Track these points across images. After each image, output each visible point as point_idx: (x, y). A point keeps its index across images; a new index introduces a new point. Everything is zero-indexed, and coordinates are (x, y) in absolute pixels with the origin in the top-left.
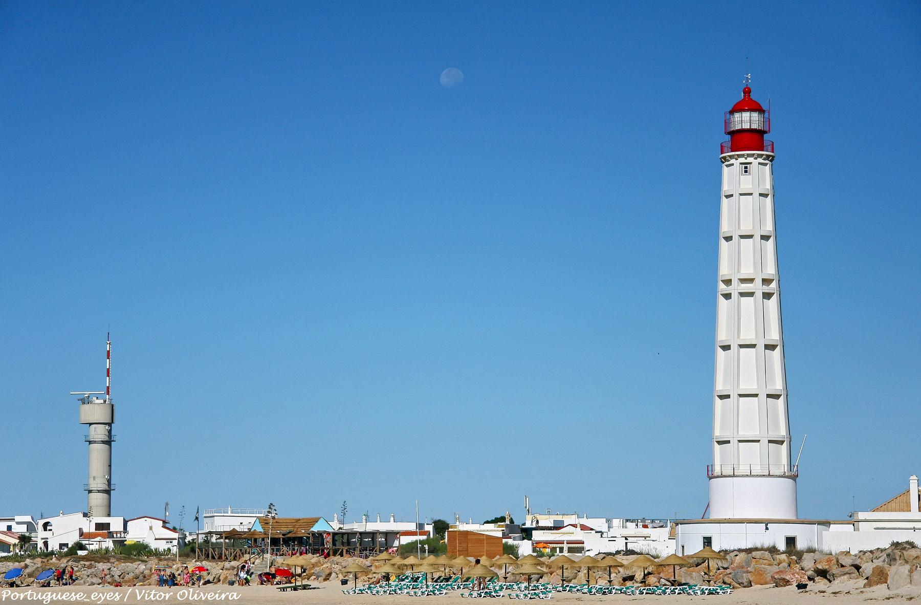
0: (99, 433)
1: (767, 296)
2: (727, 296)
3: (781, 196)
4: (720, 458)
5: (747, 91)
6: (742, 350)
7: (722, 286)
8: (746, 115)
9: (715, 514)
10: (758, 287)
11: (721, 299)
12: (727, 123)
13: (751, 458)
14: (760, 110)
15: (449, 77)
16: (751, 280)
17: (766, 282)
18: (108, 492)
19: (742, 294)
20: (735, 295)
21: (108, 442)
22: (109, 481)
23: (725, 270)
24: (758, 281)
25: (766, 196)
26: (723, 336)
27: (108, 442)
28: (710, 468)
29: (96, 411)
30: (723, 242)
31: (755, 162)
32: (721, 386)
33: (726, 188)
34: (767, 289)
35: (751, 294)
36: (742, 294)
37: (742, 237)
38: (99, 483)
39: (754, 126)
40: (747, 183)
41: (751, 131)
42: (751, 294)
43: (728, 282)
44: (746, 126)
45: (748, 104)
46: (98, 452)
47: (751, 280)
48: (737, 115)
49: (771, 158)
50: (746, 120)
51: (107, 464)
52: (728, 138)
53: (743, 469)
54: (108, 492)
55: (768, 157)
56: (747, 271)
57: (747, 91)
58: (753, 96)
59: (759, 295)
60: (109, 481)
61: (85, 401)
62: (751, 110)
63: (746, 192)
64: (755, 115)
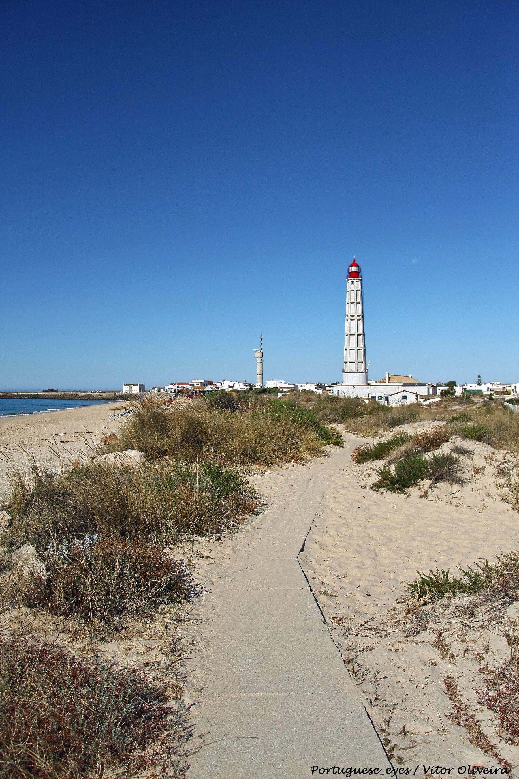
0: (259, 360)
1: (358, 320)
2: (347, 320)
5: (354, 261)
7: (346, 317)
8: (353, 267)
10: (355, 318)
12: (349, 270)
14: (357, 265)
15: (414, 261)
16: (354, 316)
17: (358, 316)
18: (262, 375)
19: (351, 320)
21: (262, 362)
22: (262, 372)
23: (347, 313)
27: (262, 362)
28: (343, 370)
29: (258, 354)
32: (346, 347)
34: (358, 318)
35: (354, 320)
36: (351, 320)
38: (260, 373)
40: (353, 287)
41: (354, 272)
42: (354, 320)
44: (353, 271)
45: (354, 264)
46: (259, 365)
47: (354, 316)
50: (354, 269)
51: (108, 390)
52: (349, 274)
53: (350, 371)
54: (262, 375)
56: (353, 312)
57: (354, 261)
58: (356, 262)
60: (262, 372)
64: (356, 267)
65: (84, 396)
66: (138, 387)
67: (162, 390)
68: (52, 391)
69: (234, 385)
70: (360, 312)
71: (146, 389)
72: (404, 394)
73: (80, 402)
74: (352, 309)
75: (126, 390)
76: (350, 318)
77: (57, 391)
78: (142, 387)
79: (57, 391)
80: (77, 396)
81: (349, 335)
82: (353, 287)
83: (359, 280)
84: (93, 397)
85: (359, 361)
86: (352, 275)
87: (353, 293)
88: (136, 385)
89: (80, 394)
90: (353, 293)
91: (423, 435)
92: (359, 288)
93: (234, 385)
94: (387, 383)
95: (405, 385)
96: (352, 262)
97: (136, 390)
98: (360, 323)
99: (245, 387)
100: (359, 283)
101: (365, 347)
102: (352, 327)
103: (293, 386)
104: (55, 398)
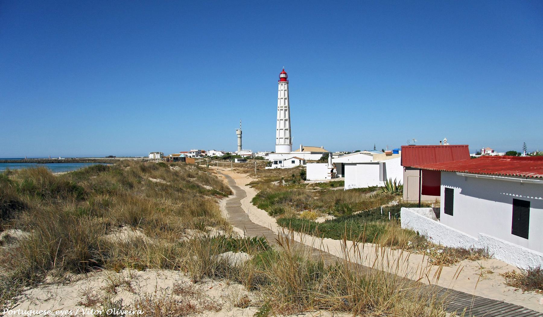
0: (239, 136)
1: (286, 110)
10: (284, 108)
14: (285, 73)
21: (241, 138)
23: (279, 105)
29: (238, 132)
38: (239, 144)
40: (282, 88)
42: (282, 110)
46: (239, 140)
49: (288, 83)
50: (283, 76)
68: (111, 157)
70: (287, 104)
72: (293, 159)
74: (281, 103)
79: (115, 157)
82: (282, 87)
85: (286, 137)
86: (285, 79)
88: (158, 153)
91: (220, 211)
92: (286, 88)
94: (301, 152)
95: (312, 153)
98: (287, 112)
100: (286, 86)
101: (290, 128)
102: (281, 115)
103: (251, 153)
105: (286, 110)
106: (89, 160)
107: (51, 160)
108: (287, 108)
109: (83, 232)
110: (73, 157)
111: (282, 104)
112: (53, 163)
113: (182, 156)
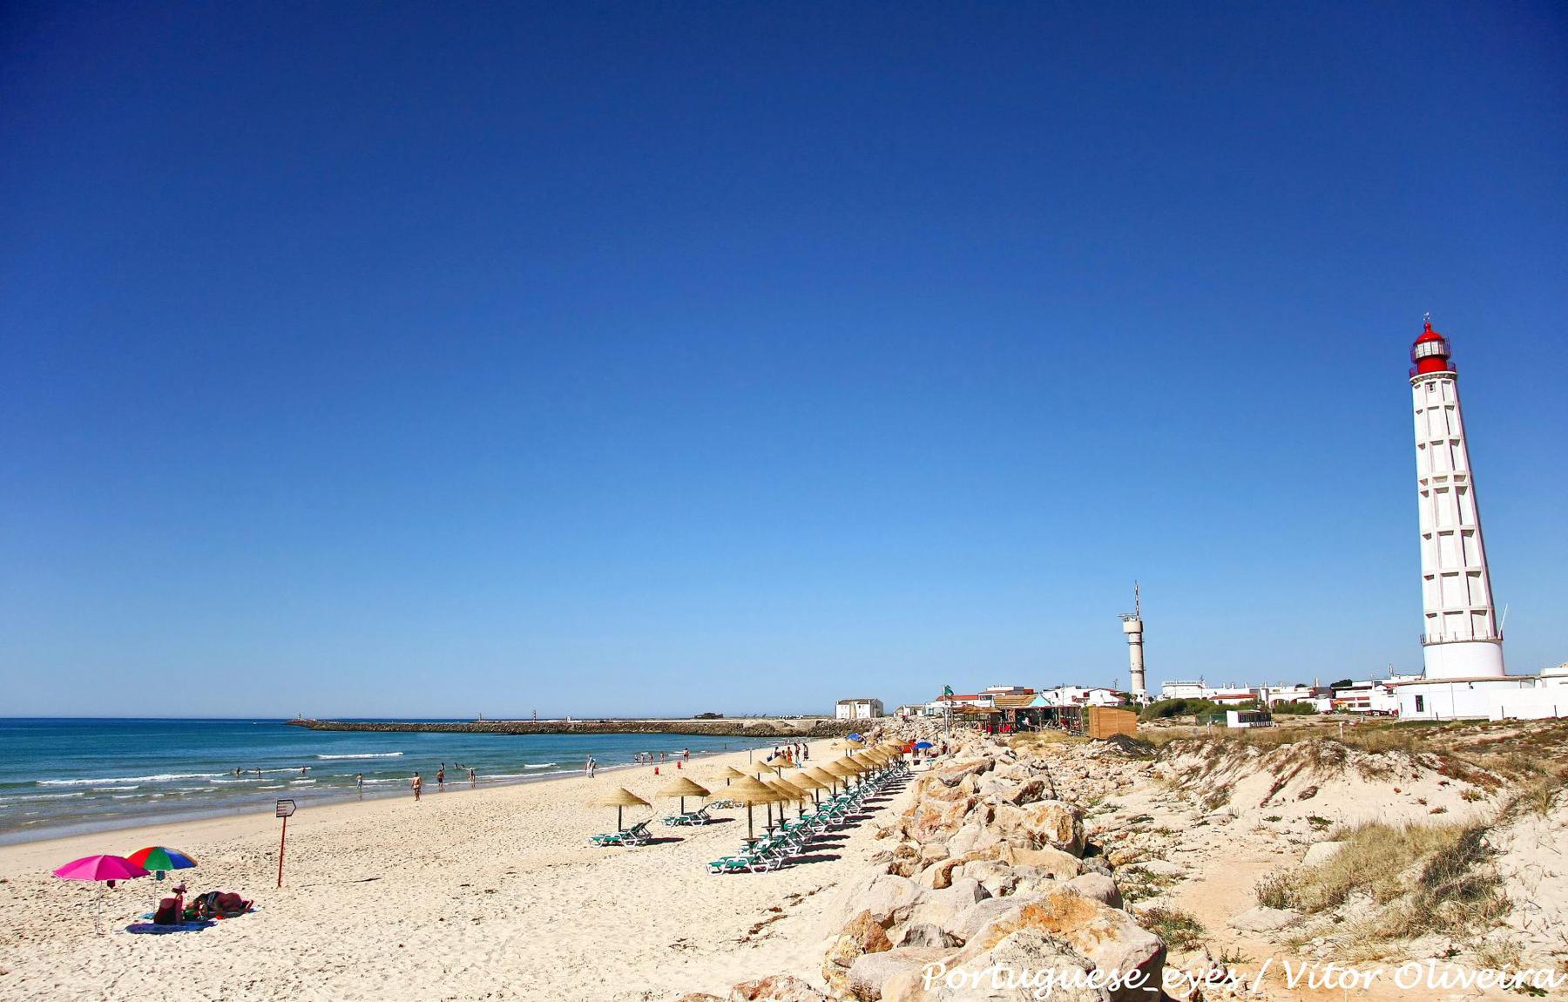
0: (1134, 638)
1: (1460, 490)
2: (1426, 493)
3: (1464, 405)
4: (1432, 629)
6: (1443, 538)
8: (1427, 345)
9: (1430, 676)
10: (1451, 484)
11: (1421, 497)
12: (1413, 354)
13: (1454, 593)
17: (1456, 477)
19: (1438, 491)
20: (1431, 493)
21: (1140, 643)
23: (1421, 474)
24: (1451, 478)
25: (1451, 408)
26: (1425, 527)
27: (1140, 643)
28: (1423, 638)
29: (1132, 626)
30: (1421, 497)
31: (1438, 381)
33: (1417, 405)
34: (1460, 484)
35: (1446, 490)
36: (1438, 491)
37: (1441, 534)
38: (1136, 667)
39: (1436, 352)
40: (1435, 398)
42: (1446, 490)
43: (1425, 482)
46: (1134, 650)
48: (1420, 347)
49: (1454, 377)
50: (1428, 349)
55: (1450, 376)
56: (1443, 468)
57: (1428, 327)
59: (1452, 490)
61: (1127, 620)
62: (1431, 340)
63: (1434, 408)
64: (1435, 344)
65: (712, 728)
66: (867, 707)
67: (920, 713)
68: (710, 716)
69: (1086, 695)
70: (1462, 467)
71: (885, 711)
73: (619, 741)
75: (843, 713)
76: (1431, 487)
77: (721, 717)
78: (877, 708)
79: (721, 717)
80: (740, 726)
81: (1434, 536)
83: (1450, 376)
84: (773, 729)
85: (1475, 607)
87: (1437, 416)
88: (862, 702)
89: (747, 723)
90: (1437, 416)
93: (1086, 695)
96: (893, 876)
97: (864, 712)
99: (1116, 700)
100: (1450, 389)
103: (1246, 691)
104: (711, 733)
105: (1460, 490)
106: (646, 726)
107: (538, 726)
108: (1466, 482)
109: (746, 786)
110: (604, 716)
111: (1443, 468)
112: (542, 732)
113: (1065, 699)
